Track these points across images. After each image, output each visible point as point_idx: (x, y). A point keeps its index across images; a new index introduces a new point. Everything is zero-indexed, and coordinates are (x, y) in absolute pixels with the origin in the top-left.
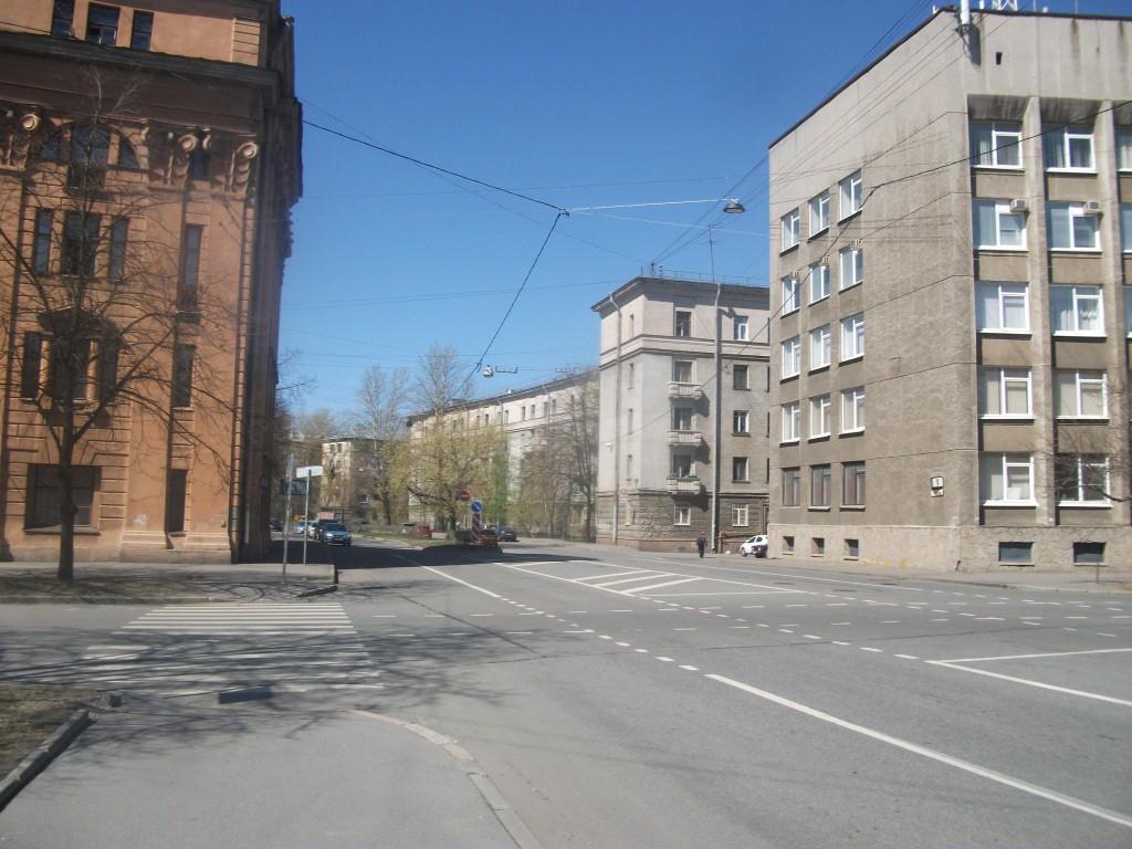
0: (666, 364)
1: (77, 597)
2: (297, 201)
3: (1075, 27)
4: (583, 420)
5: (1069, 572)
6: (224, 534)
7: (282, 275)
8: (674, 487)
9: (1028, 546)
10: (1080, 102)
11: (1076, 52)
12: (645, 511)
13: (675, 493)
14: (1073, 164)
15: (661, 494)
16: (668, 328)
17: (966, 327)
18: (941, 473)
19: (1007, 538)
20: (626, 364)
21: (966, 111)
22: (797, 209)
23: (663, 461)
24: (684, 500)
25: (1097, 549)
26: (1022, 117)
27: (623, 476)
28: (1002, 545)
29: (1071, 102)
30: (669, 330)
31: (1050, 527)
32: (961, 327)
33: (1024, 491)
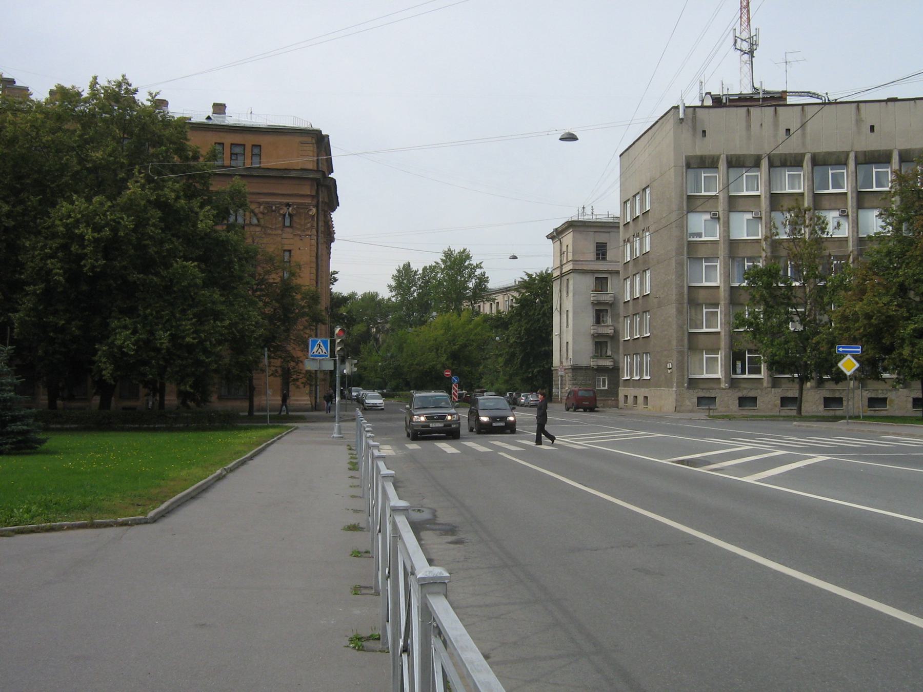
0: (588, 282)
2: (334, 181)
3: (748, 112)
4: (796, 223)
5: (691, 411)
6: (308, 398)
7: (329, 253)
8: (595, 363)
9: (755, 399)
11: (749, 127)
15: (587, 368)
19: (702, 394)
20: (565, 278)
23: (588, 346)
24: (601, 370)
27: (564, 360)
29: (744, 156)
30: (592, 256)
33: (714, 368)
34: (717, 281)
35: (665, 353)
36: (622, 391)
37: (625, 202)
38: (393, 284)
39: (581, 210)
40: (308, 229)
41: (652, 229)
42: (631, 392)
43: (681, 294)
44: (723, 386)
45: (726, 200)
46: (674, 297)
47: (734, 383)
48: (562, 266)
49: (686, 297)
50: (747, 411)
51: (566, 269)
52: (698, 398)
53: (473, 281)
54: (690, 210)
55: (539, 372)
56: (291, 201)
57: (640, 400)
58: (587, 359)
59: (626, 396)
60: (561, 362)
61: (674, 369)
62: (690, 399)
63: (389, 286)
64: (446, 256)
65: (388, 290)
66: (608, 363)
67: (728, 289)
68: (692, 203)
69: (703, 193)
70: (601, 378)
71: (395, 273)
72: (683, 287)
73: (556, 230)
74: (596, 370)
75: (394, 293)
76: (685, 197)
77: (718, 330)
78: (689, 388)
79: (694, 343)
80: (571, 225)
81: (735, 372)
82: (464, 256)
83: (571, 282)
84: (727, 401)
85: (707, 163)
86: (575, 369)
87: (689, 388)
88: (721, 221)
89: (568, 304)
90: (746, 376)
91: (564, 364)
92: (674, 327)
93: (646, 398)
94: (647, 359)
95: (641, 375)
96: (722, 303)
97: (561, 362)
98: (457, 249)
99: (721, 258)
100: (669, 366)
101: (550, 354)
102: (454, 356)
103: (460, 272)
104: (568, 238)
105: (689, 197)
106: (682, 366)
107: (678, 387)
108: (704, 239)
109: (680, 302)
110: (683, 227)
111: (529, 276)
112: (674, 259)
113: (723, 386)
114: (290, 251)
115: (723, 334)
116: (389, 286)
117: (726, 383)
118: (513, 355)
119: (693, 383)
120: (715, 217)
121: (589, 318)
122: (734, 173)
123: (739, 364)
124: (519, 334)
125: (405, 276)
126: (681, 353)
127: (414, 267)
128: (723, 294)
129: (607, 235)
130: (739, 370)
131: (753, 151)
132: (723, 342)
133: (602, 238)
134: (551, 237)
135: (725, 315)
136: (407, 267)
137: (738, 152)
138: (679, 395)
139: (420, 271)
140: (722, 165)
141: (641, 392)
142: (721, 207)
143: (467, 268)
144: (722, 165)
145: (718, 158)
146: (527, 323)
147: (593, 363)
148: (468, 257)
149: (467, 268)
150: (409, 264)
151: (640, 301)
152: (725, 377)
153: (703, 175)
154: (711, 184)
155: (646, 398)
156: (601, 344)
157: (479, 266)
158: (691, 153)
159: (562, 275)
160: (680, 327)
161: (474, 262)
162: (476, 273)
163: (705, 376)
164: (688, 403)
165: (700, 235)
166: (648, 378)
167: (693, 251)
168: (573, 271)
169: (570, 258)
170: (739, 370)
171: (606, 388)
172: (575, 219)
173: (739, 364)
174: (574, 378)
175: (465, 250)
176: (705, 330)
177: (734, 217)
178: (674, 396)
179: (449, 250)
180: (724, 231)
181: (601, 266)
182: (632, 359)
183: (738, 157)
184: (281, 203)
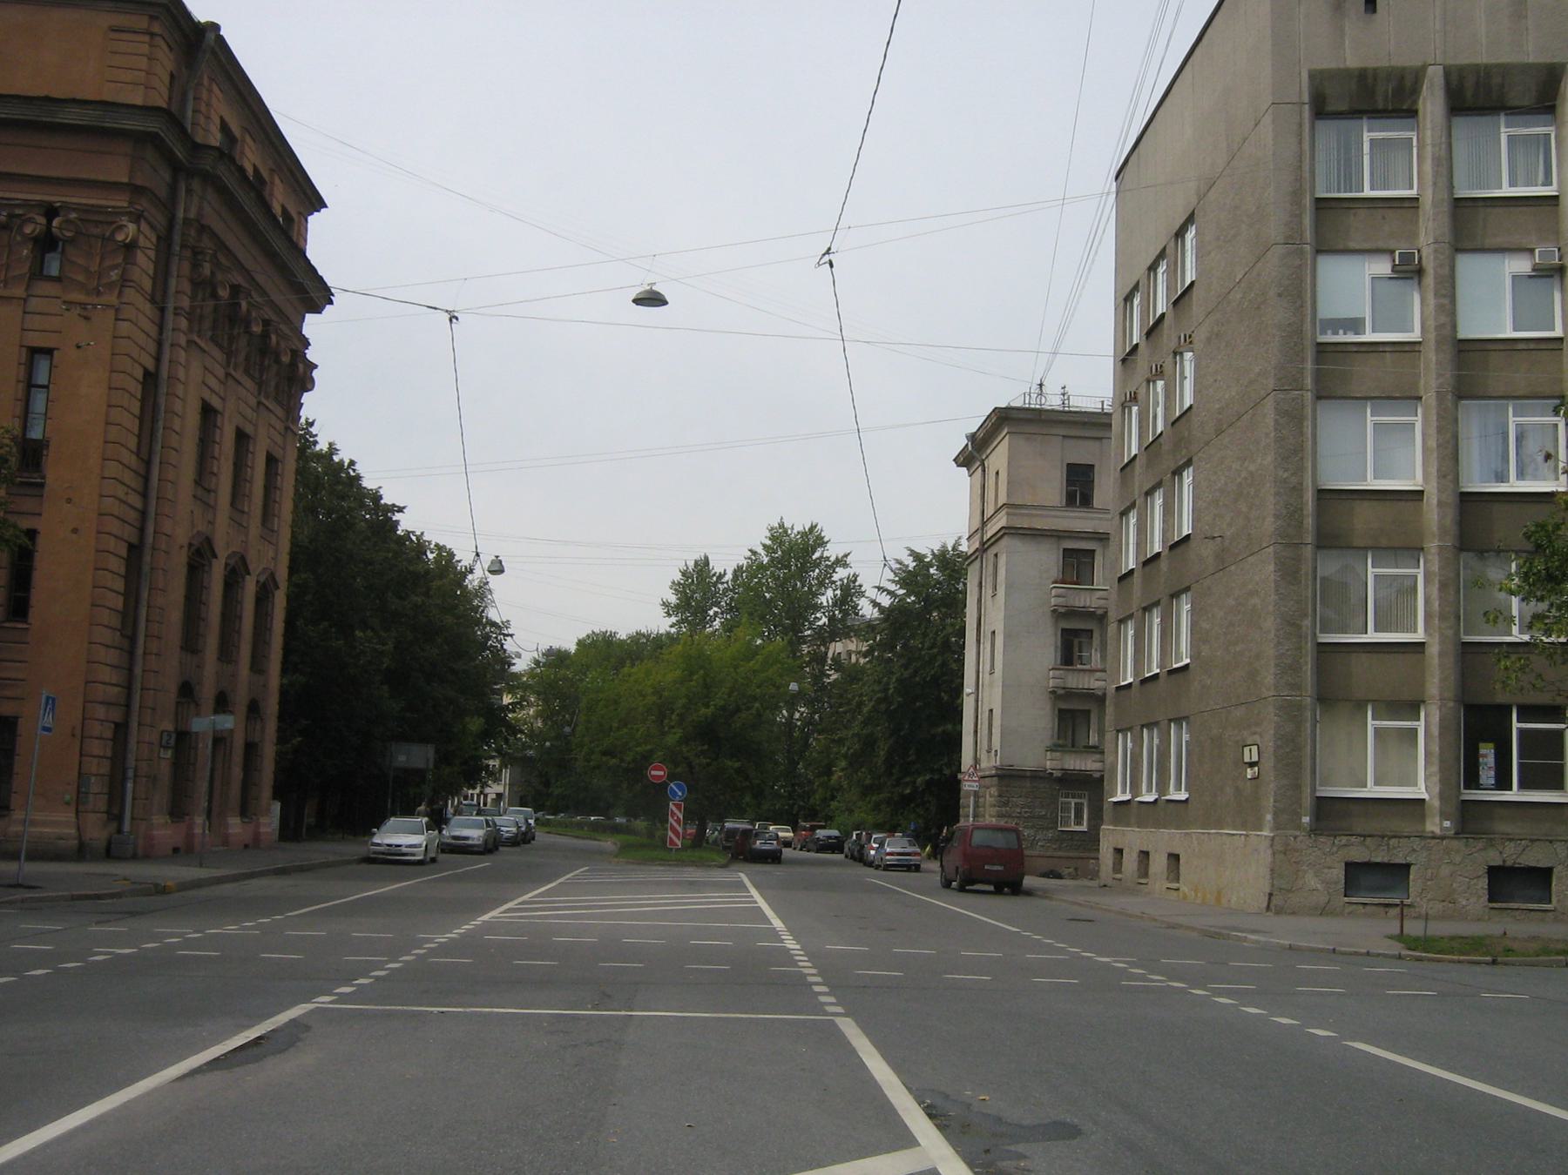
0: (1047, 559)
1: (1405, 952)
5: (1324, 911)
10: (1526, 68)
12: (1006, 804)
13: (1057, 774)
14: (1512, 184)
15: (1037, 776)
16: (1052, 489)
17: (1294, 480)
18: (1257, 738)
19: (1359, 854)
21: (1306, 98)
22: (637, 301)
23: (1039, 720)
25: (1540, 879)
26: (1415, 102)
27: (983, 756)
28: (1351, 868)
29: (1505, 70)
31: (1443, 838)
32: (1285, 481)
33: (1398, 764)
34: (1409, 471)
35: (1239, 713)
36: (1110, 837)
37: (1128, 299)
38: (673, 599)
39: (1035, 389)
40: (111, 285)
41: (1200, 336)
42: (1133, 838)
43: (1292, 514)
44: (1433, 825)
45: (1446, 208)
46: (1269, 525)
47: (1471, 820)
48: (984, 524)
49: (1309, 522)
50: (1518, 924)
51: (991, 530)
52: (1350, 866)
53: (830, 593)
54: (1324, 247)
55: (929, 783)
56: (56, 197)
57: (1158, 863)
58: (1035, 755)
59: (1119, 852)
60: (976, 760)
61: (1268, 764)
62: (1322, 870)
63: (665, 604)
64: (773, 538)
65: (661, 612)
66: (1088, 764)
67: (1451, 499)
68: (1332, 223)
69: (1368, 193)
70: (1073, 802)
71: (678, 577)
72: (1298, 489)
73: (972, 437)
74: (1060, 780)
75: (674, 619)
76: (1308, 201)
77: (1419, 636)
78: (1315, 831)
79: (1337, 682)
80: (1003, 419)
81: (1472, 781)
82: (812, 540)
83: (1002, 560)
84: (1449, 886)
85: (1378, 96)
86: (1007, 777)
87: (1315, 831)
88: (1429, 280)
89: (996, 618)
90: (1514, 795)
91: (984, 764)
92: (1270, 623)
93: (1174, 858)
94: (1180, 738)
95: (1162, 787)
96: (1432, 545)
97: (976, 760)
98: (798, 523)
99: (1430, 397)
100: (1251, 754)
101: (955, 742)
102: (710, 735)
103: (803, 570)
104: (998, 457)
105: (1321, 204)
106: (1293, 758)
107: (1277, 826)
108: (1369, 336)
109: (1289, 542)
110: (1300, 296)
111: (918, 557)
112: (1269, 406)
113: (1433, 825)
114: (49, 352)
115: (1434, 650)
116: (665, 604)
117: (1444, 815)
118: (869, 743)
119: (1332, 815)
120: (1409, 271)
121: (1045, 650)
122: (1464, 127)
123: (1487, 753)
124: (886, 690)
125: (696, 590)
126: (1292, 712)
127: (717, 566)
128: (1435, 517)
129: (1097, 443)
130: (1487, 775)
131: (1533, 51)
132: (1437, 679)
133: (1081, 453)
134: (966, 460)
135: (1443, 586)
136: (703, 565)
137: (1483, 58)
138: (1283, 851)
139: (729, 577)
140: (1432, 103)
141: (1161, 841)
142: (1429, 234)
143: (817, 564)
144: (1432, 103)
145: (1418, 74)
146: (906, 667)
147: (1051, 763)
148: (821, 542)
149: (817, 564)
150: (706, 561)
151: (1163, 565)
152: (1442, 796)
153: (1367, 136)
154: (1391, 164)
155: (1174, 858)
156: (1074, 715)
157: (841, 562)
158: (1328, 63)
159: (984, 548)
160: (1291, 625)
161: (832, 552)
162: (836, 577)
163: (1372, 791)
164: (1311, 881)
165: (1355, 325)
166: (1183, 796)
167: (1335, 371)
168: (1007, 531)
169: (1002, 500)
170: (1487, 775)
171: (1084, 828)
172: (1018, 403)
173: (1487, 753)
174: (1003, 801)
175: (813, 528)
176: (1372, 636)
177: (1469, 266)
178: (1266, 857)
179: (781, 525)
180: (1440, 308)
181: (1078, 521)
182: (1138, 742)
183: (1483, 75)
184: (26, 204)
